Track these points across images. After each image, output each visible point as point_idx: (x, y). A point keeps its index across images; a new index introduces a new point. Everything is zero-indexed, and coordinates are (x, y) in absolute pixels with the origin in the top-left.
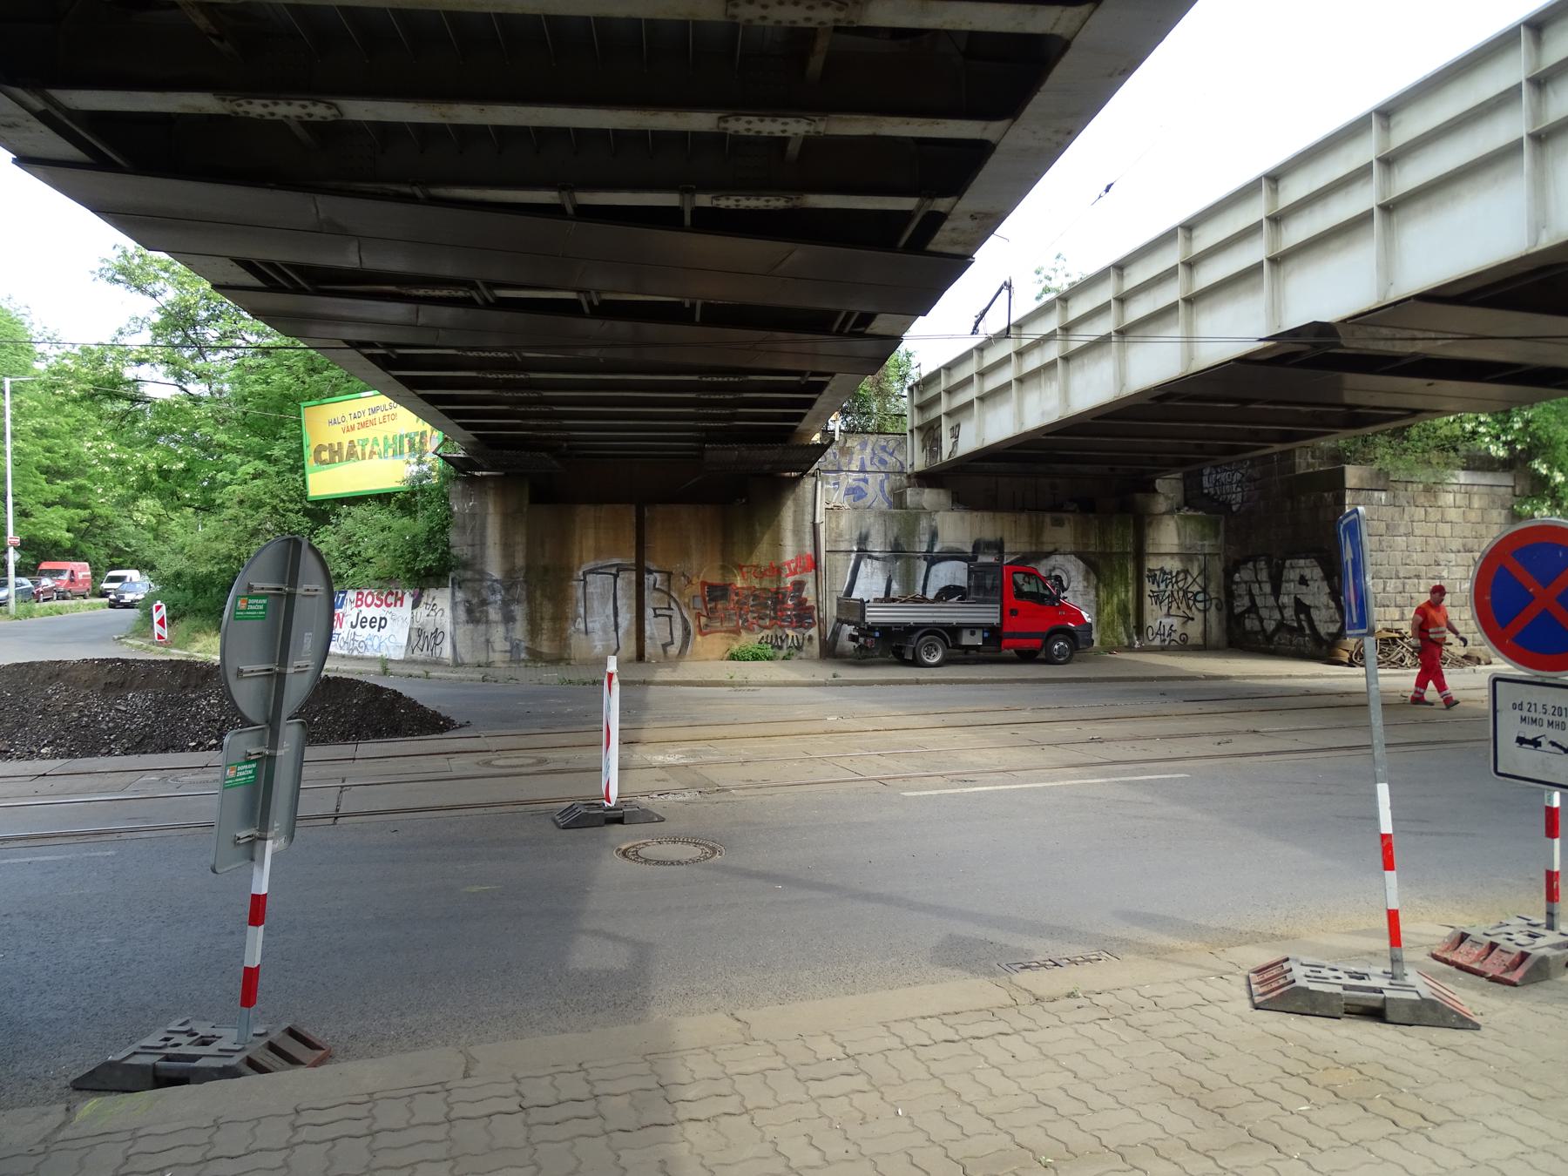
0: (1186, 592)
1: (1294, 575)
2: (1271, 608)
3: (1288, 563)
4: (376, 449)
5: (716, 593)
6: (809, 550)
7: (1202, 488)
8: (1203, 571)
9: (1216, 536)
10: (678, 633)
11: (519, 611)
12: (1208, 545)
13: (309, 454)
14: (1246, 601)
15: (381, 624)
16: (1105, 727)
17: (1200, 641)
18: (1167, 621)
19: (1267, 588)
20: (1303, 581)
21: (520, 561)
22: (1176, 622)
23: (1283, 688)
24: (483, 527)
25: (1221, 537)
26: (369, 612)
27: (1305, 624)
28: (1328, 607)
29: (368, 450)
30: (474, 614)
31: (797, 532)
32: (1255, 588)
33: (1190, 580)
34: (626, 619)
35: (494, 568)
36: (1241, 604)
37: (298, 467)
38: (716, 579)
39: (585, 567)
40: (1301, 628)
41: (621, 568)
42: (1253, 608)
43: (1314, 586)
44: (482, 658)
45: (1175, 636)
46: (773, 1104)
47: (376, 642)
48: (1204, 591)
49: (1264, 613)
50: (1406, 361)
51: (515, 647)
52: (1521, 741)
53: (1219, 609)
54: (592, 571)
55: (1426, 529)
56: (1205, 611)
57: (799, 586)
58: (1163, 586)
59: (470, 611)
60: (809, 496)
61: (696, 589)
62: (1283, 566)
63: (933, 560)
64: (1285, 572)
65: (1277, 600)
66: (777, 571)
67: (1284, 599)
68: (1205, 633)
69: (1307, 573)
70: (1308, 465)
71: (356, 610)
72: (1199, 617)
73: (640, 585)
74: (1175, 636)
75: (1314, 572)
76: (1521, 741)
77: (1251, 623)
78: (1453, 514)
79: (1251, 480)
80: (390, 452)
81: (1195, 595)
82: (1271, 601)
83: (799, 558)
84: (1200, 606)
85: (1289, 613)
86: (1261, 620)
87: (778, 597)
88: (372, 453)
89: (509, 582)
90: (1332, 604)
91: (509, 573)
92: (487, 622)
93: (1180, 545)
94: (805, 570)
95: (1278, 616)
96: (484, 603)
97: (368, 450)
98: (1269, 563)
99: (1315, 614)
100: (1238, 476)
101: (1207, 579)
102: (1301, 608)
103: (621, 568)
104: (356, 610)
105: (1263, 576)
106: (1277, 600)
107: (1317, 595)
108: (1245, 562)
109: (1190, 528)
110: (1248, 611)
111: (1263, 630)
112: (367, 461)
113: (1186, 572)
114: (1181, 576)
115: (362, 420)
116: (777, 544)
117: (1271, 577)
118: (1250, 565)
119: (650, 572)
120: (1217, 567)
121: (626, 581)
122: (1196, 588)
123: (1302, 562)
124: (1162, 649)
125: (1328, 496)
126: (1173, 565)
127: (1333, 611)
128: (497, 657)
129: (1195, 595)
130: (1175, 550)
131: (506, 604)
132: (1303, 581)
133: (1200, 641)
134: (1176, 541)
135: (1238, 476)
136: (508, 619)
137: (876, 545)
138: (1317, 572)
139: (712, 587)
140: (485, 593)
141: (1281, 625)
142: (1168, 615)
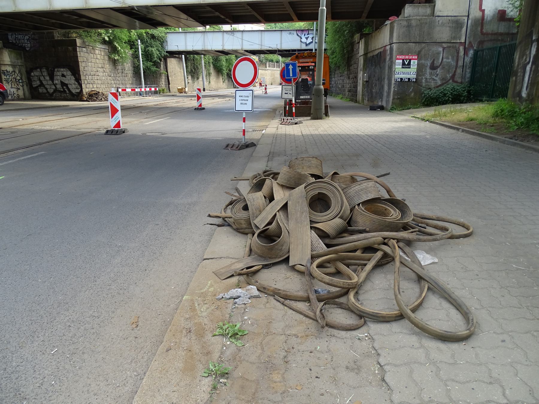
0: (16, 79)
1: (59, 74)
2: (50, 85)
3: (56, 70)
7: (8, 39)
8: (20, 72)
9: (21, 59)
12: (19, 62)
14: (38, 83)
17: (23, 97)
18: (12, 90)
19: (48, 78)
20: (63, 76)
22: (15, 90)
23: (102, 106)
25: (23, 59)
27: (66, 90)
28: (75, 84)
32: (42, 78)
33: (16, 75)
36: (36, 84)
40: (65, 91)
42: (42, 85)
43: (68, 77)
45: (15, 95)
48: (21, 79)
49: (47, 87)
50: (154, 21)
52: (241, 104)
53: (27, 86)
55: (94, 61)
56: (23, 86)
58: (8, 77)
62: (54, 71)
64: (55, 73)
65: (53, 82)
67: (56, 82)
68: (24, 94)
69: (65, 73)
70: (58, 37)
72: (21, 88)
74: (15, 95)
75: (68, 73)
76: (241, 104)
77: (41, 90)
78: (99, 57)
79: (33, 39)
81: (19, 80)
82: (50, 82)
84: (21, 84)
85: (59, 86)
86: (46, 89)
90: (76, 83)
93: (11, 61)
95: (54, 87)
98: (47, 69)
99: (70, 86)
100: (27, 37)
101: (21, 74)
102: (63, 84)
105: (45, 74)
106: (53, 82)
107: (70, 80)
108: (36, 68)
109: (13, 55)
110: (40, 86)
111: (48, 92)
113: (14, 72)
114: (13, 73)
117: (49, 74)
118: (39, 70)
120: (24, 70)
122: (18, 78)
123: (62, 69)
124: (13, 100)
126: (10, 69)
127: (77, 85)
129: (19, 80)
130: (9, 63)
132: (63, 76)
133: (23, 97)
134: (9, 60)
135: (27, 37)
138: (69, 73)
141: (56, 90)
142: (12, 88)
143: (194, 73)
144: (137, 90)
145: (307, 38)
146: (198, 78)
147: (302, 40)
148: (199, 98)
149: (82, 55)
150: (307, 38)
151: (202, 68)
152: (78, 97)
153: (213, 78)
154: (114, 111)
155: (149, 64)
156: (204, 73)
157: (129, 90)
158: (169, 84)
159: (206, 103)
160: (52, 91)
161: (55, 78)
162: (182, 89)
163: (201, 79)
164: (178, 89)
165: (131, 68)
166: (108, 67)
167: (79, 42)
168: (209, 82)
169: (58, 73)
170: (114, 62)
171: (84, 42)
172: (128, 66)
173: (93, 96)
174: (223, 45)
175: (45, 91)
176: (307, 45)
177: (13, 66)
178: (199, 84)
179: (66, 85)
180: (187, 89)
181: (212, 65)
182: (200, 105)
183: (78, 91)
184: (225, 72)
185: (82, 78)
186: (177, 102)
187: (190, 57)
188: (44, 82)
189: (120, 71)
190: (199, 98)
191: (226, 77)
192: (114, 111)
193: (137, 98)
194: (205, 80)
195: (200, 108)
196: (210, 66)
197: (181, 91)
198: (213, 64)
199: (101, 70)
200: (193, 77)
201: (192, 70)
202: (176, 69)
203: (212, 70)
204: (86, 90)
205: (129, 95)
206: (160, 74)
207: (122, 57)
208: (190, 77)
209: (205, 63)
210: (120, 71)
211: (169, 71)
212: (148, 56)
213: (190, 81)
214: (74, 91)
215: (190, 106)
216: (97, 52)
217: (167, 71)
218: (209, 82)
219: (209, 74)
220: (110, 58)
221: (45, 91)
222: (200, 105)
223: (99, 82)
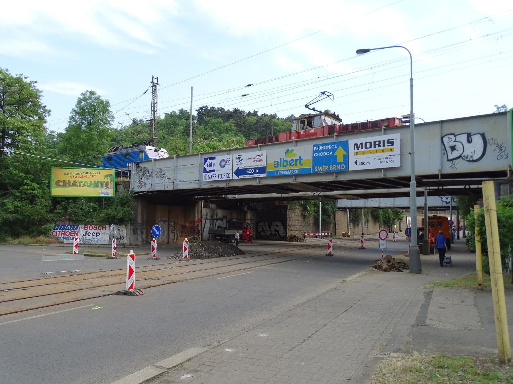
1: (275, 224)
4: (86, 184)
5: (183, 227)
6: (200, 218)
10: (176, 237)
11: (145, 231)
13: (53, 183)
14: (261, 229)
15: (98, 234)
16: (68, 285)
19: (267, 227)
20: (277, 226)
21: (145, 218)
24: (137, 210)
26: (91, 232)
29: (82, 184)
30: (135, 232)
31: (198, 213)
32: (264, 227)
34: (166, 234)
35: (139, 221)
36: (260, 230)
37: (49, 186)
38: (183, 224)
39: (158, 220)
40: (276, 235)
41: (165, 221)
42: (263, 230)
44: (136, 243)
46: (378, 238)
47: (96, 240)
49: (266, 232)
51: (143, 241)
54: (159, 222)
57: (198, 225)
59: (134, 231)
60: (200, 205)
61: (179, 226)
63: (217, 220)
66: (194, 222)
67: (272, 229)
69: (278, 224)
71: (85, 231)
73: (169, 225)
80: (93, 186)
83: (198, 219)
86: (266, 233)
87: (194, 228)
88: (84, 185)
89: (142, 224)
91: (142, 221)
92: (138, 234)
94: (199, 222)
96: (137, 229)
97: (82, 184)
99: (280, 232)
102: (276, 231)
103: (165, 221)
104: (85, 231)
105: (266, 224)
107: (280, 228)
112: (82, 187)
115: (80, 175)
116: (194, 216)
119: (171, 222)
121: (167, 223)
125: (284, 210)
126: (249, 222)
128: (139, 243)
131: (142, 230)
132: (277, 226)
136: (142, 233)
137: (209, 216)
138: (281, 224)
139: (182, 226)
140: (137, 226)
141: (271, 234)
143: (355, 221)
144: (316, 234)
145: (447, 198)
146: (358, 225)
147: (443, 200)
148: (362, 242)
149: (289, 213)
150: (447, 198)
151: (361, 217)
152: (284, 238)
153: (371, 224)
154: (330, 247)
155: (325, 217)
156: (364, 221)
157: (311, 234)
158: (336, 229)
159: (366, 244)
160: (269, 234)
161: (272, 227)
162: (345, 234)
163: (360, 225)
164: (343, 234)
165: (313, 219)
166: (301, 219)
167: (289, 206)
168: (367, 228)
169: (274, 224)
170: (304, 216)
171: (291, 206)
172: (311, 219)
173: (293, 238)
174: (379, 204)
175: (264, 234)
176: (447, 203)
177: (251, 220)
178: (359, 229)
179: (278, 231)
180: (349, 234)
181: (370, 214)
182: (363, 246)
183: (284, 235)
184: (382, 219)
185: (288, 227)
186: (346, 244)
187: (355, 215)
188: (265, 229)
189: (306, 222)
190: (362, 242)
191: (382, 223)
192: (330, 247)
193: (316, 240)
194: (364, 226)
195: (362, 248)
196: (368, 215)
197: (344, 235)
198: (371, 214)
199: (297, 222)
200: (354, 224)
201: (353, 219)
202: (342, 221)
203: (370, 218)
204: (289, 234)
205: (311, 237)
206: (331, 222)
207: (309, 214)
208: (352, 224)
209: (364, 213)
210: (306, 222)
211: (336, 220)
212: (325, 212)
213: (352, 227)
214: (281, 235)
215: (356, 246)
216: (296, 211)
217: (335, 220)
218: (367, 228)
219: (367, 221)
220: (302, 214)
221: (264, 234)
222: (363, 246)
223: (295, 229)
